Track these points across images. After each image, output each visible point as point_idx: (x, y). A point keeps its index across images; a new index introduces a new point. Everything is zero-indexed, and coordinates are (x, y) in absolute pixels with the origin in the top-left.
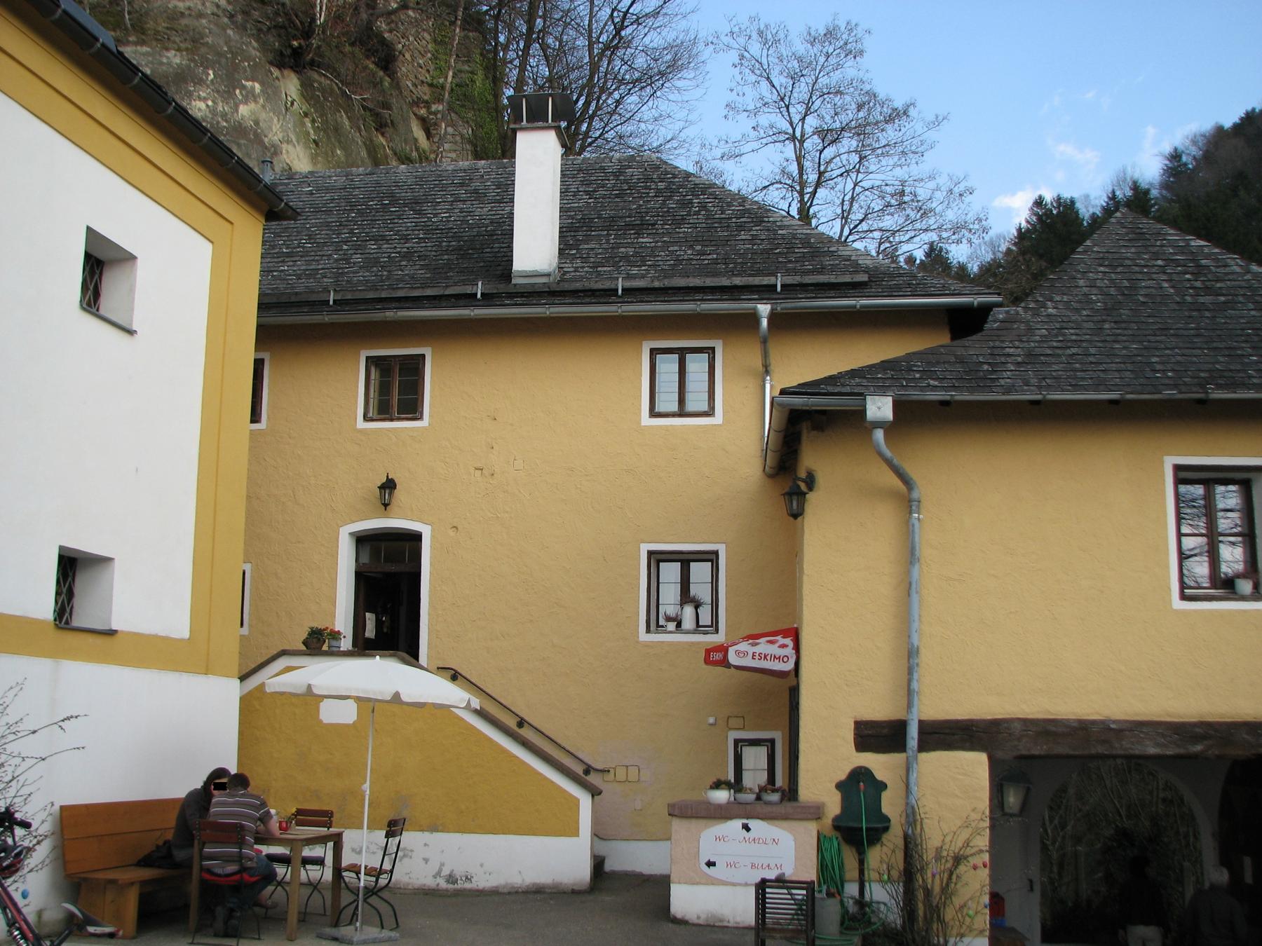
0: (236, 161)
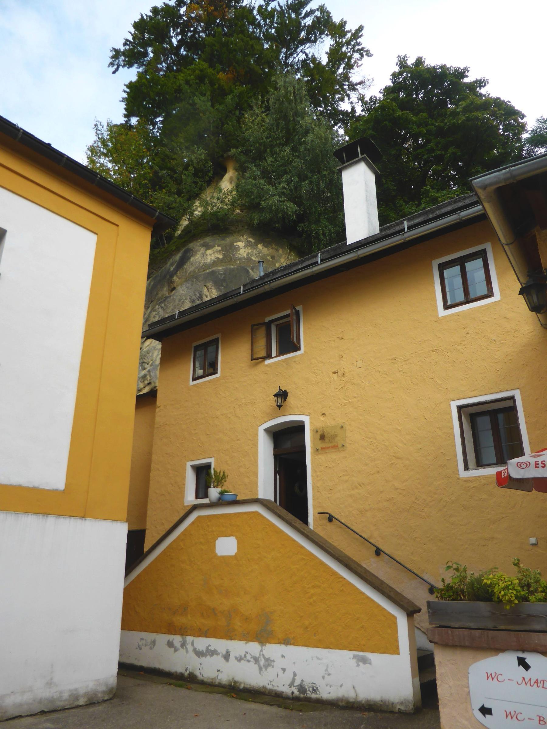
0: (100, 178)
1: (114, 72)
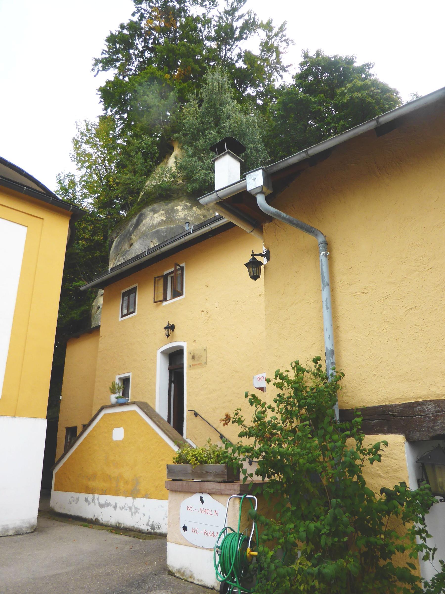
1: (95, 76)
